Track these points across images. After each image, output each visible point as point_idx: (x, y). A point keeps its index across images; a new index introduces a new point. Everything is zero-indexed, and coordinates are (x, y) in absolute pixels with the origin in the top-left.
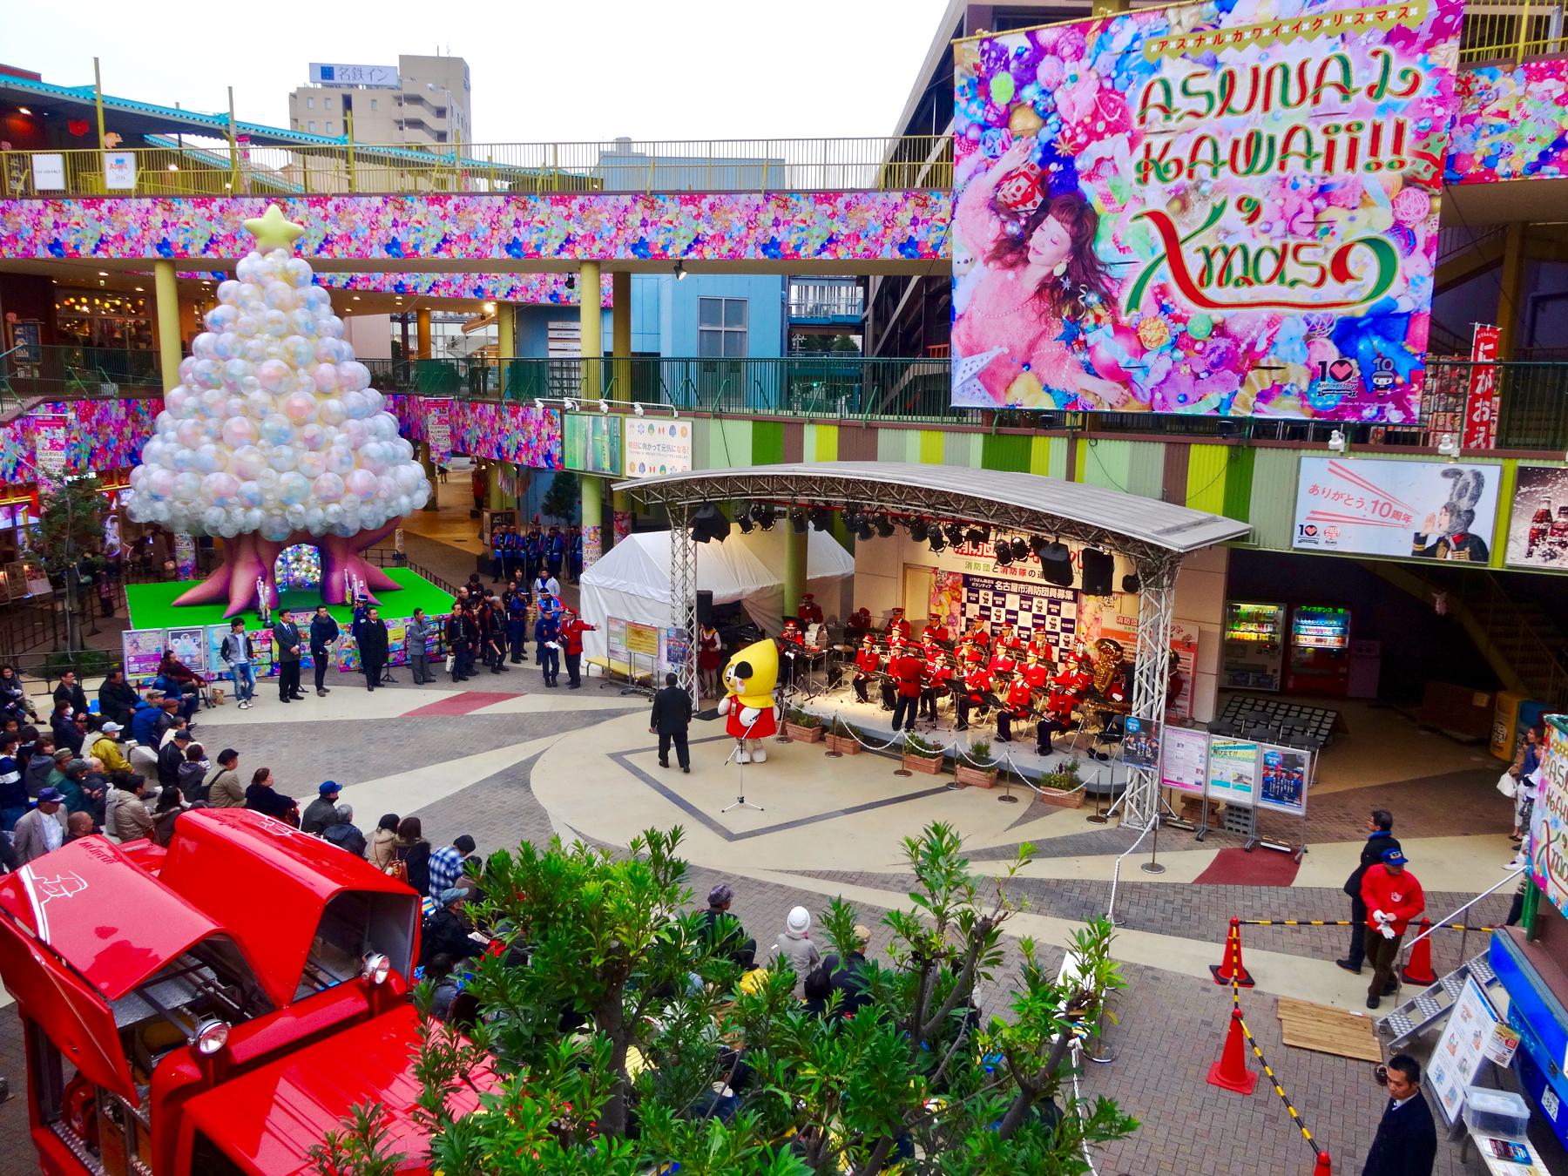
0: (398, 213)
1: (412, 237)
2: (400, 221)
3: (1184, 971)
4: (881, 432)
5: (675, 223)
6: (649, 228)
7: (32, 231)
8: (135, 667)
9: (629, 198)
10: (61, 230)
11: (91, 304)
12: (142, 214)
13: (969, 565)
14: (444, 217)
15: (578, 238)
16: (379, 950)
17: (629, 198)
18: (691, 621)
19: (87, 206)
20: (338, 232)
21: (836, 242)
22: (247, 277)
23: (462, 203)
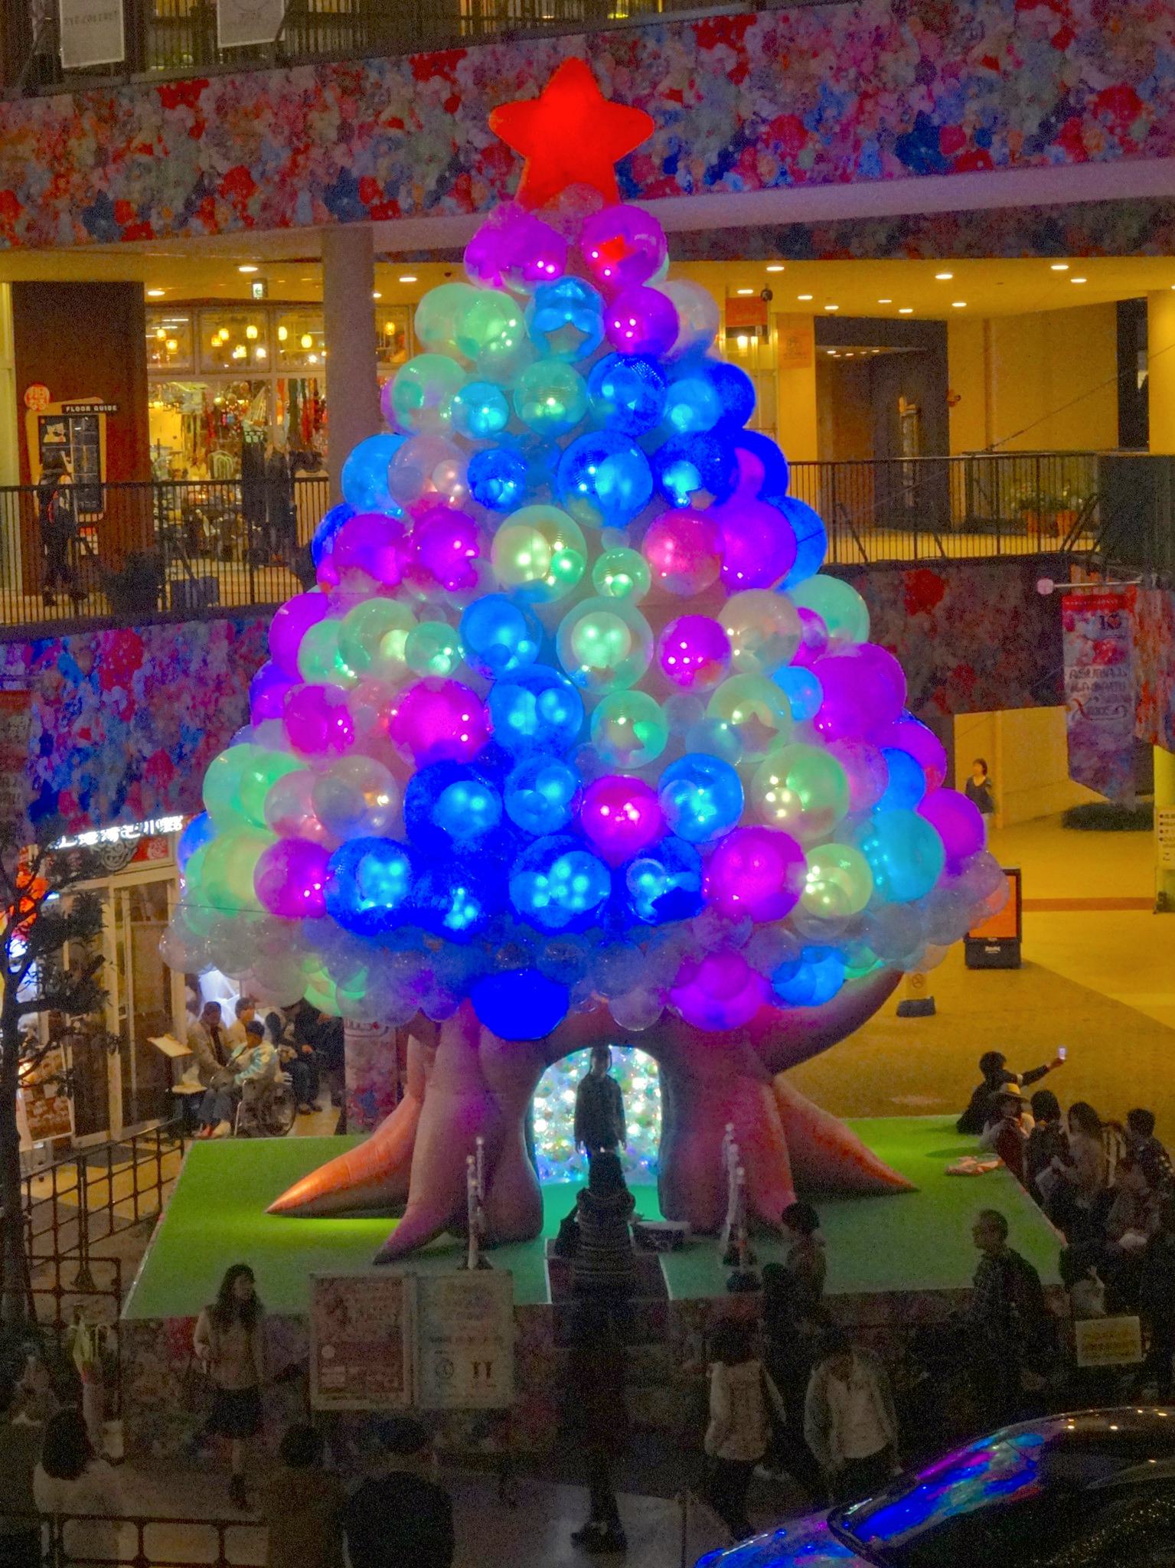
0: (931, 41)
2: (939, 64)
6: (938, 88)
14: (738, 74)
18: (872, 1396)
20: (769, 111)
22: (756, 243)
23: (782, 28)
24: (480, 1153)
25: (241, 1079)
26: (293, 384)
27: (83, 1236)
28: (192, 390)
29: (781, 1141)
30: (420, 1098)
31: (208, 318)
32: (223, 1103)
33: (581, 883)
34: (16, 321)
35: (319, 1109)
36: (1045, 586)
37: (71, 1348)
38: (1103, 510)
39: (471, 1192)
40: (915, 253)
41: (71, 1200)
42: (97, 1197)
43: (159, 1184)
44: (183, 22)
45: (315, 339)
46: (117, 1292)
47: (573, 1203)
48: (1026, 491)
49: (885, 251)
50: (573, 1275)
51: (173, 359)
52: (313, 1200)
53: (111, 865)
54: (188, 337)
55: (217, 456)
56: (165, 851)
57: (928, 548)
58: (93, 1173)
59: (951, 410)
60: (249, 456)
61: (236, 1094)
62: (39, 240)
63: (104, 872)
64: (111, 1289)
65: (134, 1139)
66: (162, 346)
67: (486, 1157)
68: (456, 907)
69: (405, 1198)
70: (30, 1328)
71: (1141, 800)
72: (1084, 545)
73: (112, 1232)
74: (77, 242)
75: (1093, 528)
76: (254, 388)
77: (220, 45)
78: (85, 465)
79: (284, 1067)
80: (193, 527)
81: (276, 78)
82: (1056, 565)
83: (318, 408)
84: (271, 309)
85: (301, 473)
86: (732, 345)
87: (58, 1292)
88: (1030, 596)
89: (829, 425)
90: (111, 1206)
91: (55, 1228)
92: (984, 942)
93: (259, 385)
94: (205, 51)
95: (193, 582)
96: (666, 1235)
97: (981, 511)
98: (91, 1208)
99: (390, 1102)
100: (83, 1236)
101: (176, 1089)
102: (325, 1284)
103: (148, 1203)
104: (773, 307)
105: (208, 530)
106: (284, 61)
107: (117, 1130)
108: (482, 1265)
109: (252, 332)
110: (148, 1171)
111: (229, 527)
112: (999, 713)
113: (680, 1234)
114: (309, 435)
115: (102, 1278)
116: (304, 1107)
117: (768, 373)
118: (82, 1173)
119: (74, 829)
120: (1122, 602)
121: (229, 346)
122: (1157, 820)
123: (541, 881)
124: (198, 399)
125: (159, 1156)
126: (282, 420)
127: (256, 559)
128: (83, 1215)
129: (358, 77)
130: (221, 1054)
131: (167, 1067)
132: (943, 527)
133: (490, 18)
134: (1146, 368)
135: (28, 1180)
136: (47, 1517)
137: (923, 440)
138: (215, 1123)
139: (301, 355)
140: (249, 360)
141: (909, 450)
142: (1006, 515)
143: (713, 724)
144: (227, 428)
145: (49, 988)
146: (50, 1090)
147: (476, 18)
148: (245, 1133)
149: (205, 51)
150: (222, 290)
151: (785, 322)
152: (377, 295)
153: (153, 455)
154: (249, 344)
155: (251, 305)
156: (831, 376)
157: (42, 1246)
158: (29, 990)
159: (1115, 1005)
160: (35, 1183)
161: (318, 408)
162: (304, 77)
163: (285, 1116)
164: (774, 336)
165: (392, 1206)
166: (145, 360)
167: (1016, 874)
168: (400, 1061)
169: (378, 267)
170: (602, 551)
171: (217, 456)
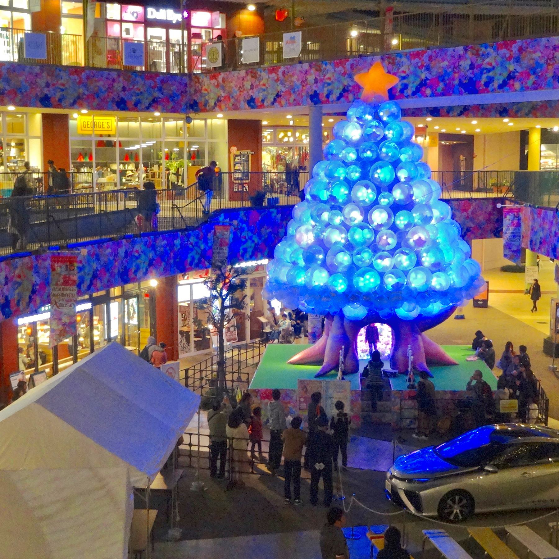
1: (261, 95)
3: (283, 489)
4: (533, 166)
5: (267, 85)
7: (238, 92)
9: (115, 73)
12: (110, 82)
13: (115, 318)
15: (282, 94)
16: (535, 402)
17: (115, 73)
21: (220, 101)
22: (425, 112)
24: (343, 350)
25: (281, 329)
26: (300, 148)
27: (239, 367)
28: (273, 149)
29: (423, 350)
30: (328, 335)
31: (278, 130)
32: (276, 335)
33: (372, 280)
34: (229, 132)
35: (301, 337)
36: (499, 206)
37: (235, 396)
38: (515, 187)
39: (340, 360)
40: (467, 116)
41: (236, 358)
42: (243, 357)
43: (259, 355)
44: (275, 52)
45: (306, 136)
46: (248, 382)
47: (367, 363)
48: (494, 181)
49: (461, 114)
50: (367, 382)
51: (269, 141)
52: (299, 360)
53: (249, 272)
54: (272, 136)
55: (279, 167)
56: (263, 269)
57: (467, 195)
58: (242, 351)
59: (474, 159)
60: (287, 166)
61: (279, 333)
62: (235, 108)
63: (247, 274)
64: (246, 381)
65: (253, 343)
66: (266, 137)
67: (345, 351)
68: (339, 285)
69: (323, 361)
70: (226, 390)
71: (523, 264)
72: (510, 195)
73: (247, 367)
74: (245, 109)
75: (511, 191)
76: (289, 149)
77: (284, 58)
78: (245, 167)
79: (292, 326)
80: (272, 185)
81: (298, 67)
82: (502, 200)
83: (306, 154)
84: (295, 128)
85: (301, 171)
86: (416, 140)
87: (233, 381)
88: (495, 208)
89: (441, 162)
90: (247, 360)
91: (232, 365)
92: (478, 301)
93: (291, 148)
94: (279, 60)
95: (273, 198)
96: (391, 373)
97: (481, 186)
98: (241, 360)
99: (320, 336)
100: (239, 367)
101: (264, 331)
102: (301, 382)
103: (256, 360)
104: (428, 130)
105: (277, 186)
106: (301, 62)
107: (248, 340)
108: (343, 379)
109: (289, 134)
110: (256, 351)
111: (281, 186)
112: (484, 240)
113: (395, 373)
114: (303, 162)
115: (244, 378)
116: (297, 337)
117: (426, 148)
118: (239, 351)
119: (239, 261)
120: (519, 210)
121: (283, 137)
122: (526, 270)
123: (362, 279)
124: (275, 151)
125: (259, 347)
126: (296, 157)
127: (289, 194)
128: (239, 362)
129: (320, 67)
130: (276, 322)
131: (262, 325)
132: (471, 190)
133: (355, 52)
134: (528, 149)
135: (226, 352)
136: (229, 438)
137: (467, 168)
138: (274, 340)
139: (302, 141)
140: (288, 141)
141: (463, 170)
142: (488, 187)
143: (409, 239)
144: (282, 159)
145: (233, 303)
146: (232, 329)
147: (351, 51)
148: (281, 343)
149: (279, 60)
150: (282, 122)
151: (431, 134)
152: (323, 125)
153: (263, 166)
154: (289, 137)
155: (289, 127)
156: (443, 149)
157: (229, 369)
158: (227, 303)
159: (513, 318)
160: (227, 352)
161: (306, 154)
162: (306, 66)
163: (292, 339)
164: (428, 138)
165: (319, 362)
166: (261, 141)
167: (488, 282)
168: (323, 325)
169: (324, 117)
170: (381, 192)
171: (279, 167)
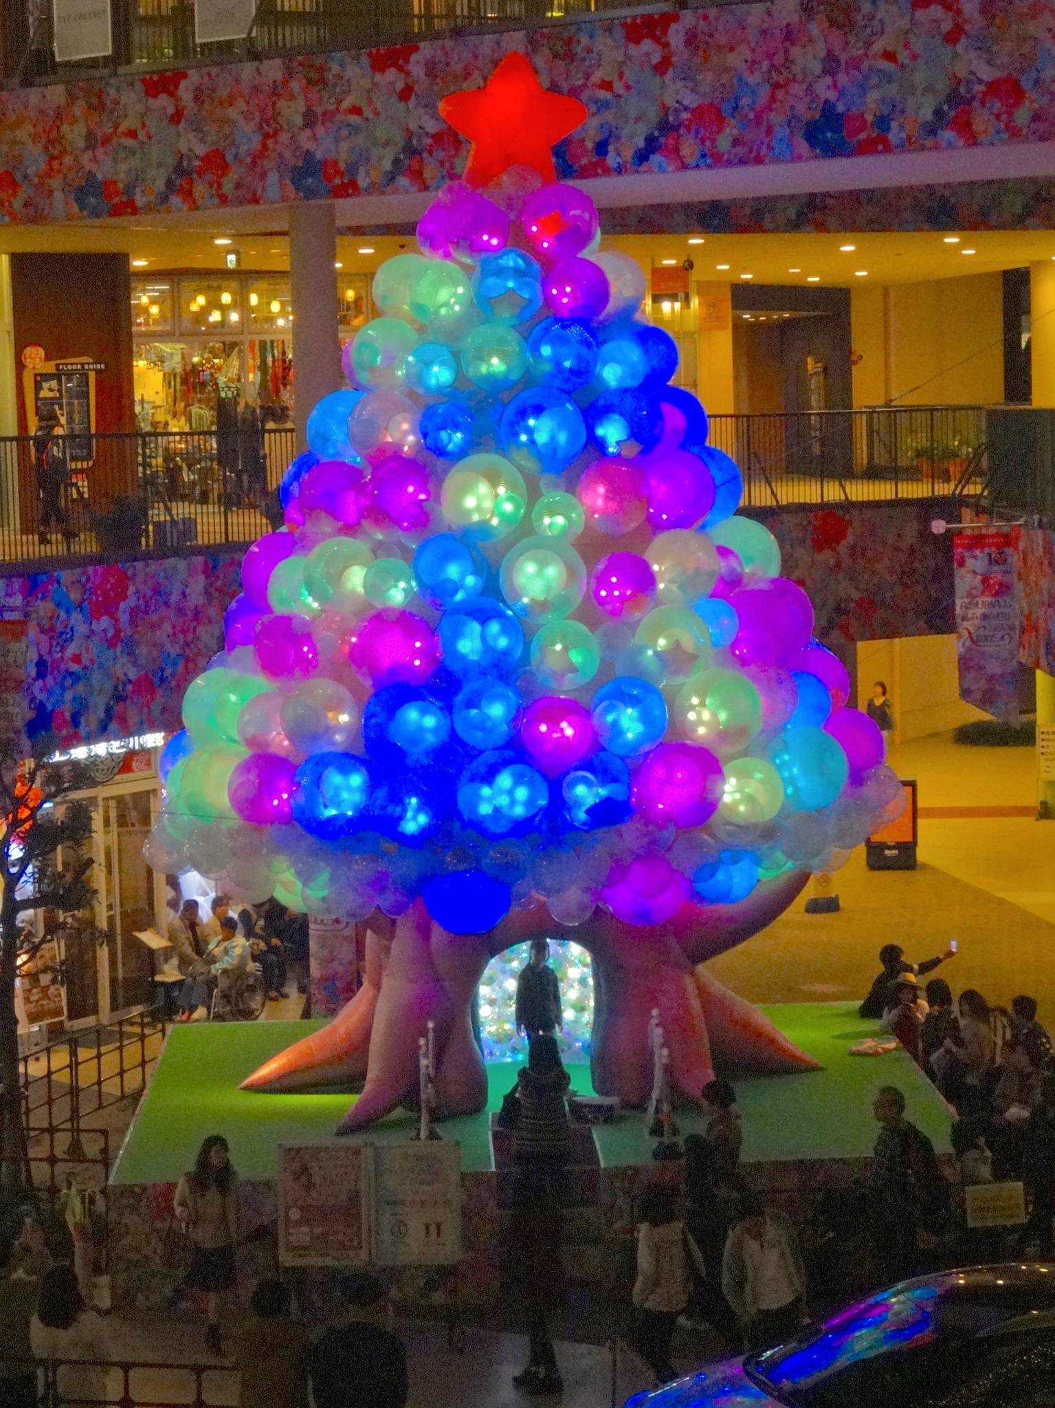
0: (836, 37)
8: (302, 1235)
10: (100, 151)
11: (241, 302)
14: (663, 67)
19: (379, 64)
